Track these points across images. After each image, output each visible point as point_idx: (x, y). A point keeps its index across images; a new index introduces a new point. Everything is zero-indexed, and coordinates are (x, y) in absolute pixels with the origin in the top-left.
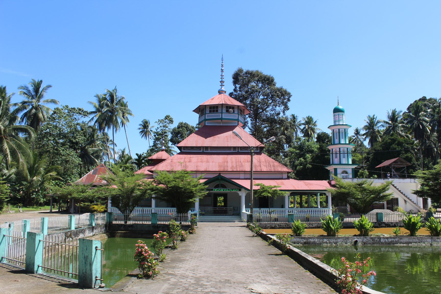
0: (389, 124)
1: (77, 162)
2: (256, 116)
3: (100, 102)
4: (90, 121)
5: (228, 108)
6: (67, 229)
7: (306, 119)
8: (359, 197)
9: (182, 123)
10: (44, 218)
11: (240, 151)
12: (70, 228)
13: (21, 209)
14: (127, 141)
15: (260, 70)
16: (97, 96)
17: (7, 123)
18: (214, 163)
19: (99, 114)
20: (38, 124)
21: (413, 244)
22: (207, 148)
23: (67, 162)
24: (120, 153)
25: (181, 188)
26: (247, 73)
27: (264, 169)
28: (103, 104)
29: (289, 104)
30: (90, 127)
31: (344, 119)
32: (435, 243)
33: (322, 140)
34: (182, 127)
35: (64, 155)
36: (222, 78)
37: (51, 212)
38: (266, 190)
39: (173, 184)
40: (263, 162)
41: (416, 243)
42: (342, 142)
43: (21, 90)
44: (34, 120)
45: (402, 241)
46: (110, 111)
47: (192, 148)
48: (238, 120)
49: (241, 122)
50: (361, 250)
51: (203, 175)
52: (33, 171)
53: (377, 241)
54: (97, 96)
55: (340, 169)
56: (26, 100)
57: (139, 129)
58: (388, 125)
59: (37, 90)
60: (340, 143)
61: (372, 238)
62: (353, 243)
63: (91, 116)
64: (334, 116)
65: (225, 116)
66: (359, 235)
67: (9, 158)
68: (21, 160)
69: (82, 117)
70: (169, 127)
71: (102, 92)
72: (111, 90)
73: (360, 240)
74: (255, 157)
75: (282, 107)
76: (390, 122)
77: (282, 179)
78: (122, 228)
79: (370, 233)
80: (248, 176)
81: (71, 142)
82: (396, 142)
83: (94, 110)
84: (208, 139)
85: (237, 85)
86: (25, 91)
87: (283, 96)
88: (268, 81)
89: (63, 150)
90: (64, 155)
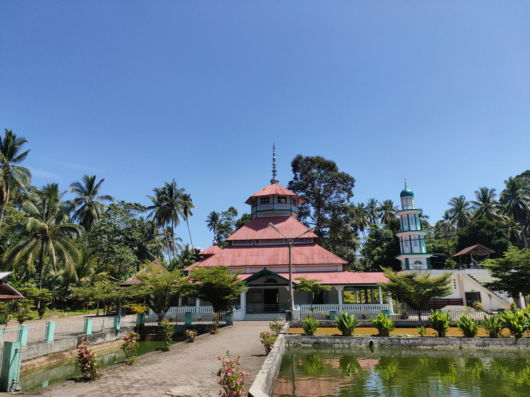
0: (480, 205)
1: (132, 259)
2: (319, 205)
3: (159, 195)
4: (147, 216)
5: (280, 198)
6: (81, 333)
7: (383, 205)
8: (412, 291)
9: (246, 215)
10: (49, 323)
11: (233, 245)
12: (85, 333)
13: (66, 314)
14: (193, 233)
15: (321, 156)
16: (156, 190)
17: (54, 222)
18: (264, 257)
19: (157, 208)
20: (91, 221)
21: (438, 346)
22: (257, 241)
23: (121, 260)
24: (184, 248)
25: (215, 284)
26: (307, 159)
27: (317, 261)
28: (162, 198)
29: (353, 190)
30: (149, 222)
31: (413, 203)
32: (466, 345)
33: (396, 226)
34: (246, 218)
35: (118, 253)
36: (274, 168)
37: (98, 316)
38: (306, 285)
39: (206, 280)
40: (318, 254)
41: (442, 345)
42: (413, 228)
43: (73, 187)
44: (87, 218)
45: (425, 342)
46: (170, 204)
47: (243, 241)
48: (291, 210)
49: (295, 212)
50: (378, 352)
51: (248, 270)
52: (82, 271)
53: (397, 344)
54: (156, 190)
55: (412, 259)
56: (79, 197)
57: (208, 221)
58: (479, 207)
59: (90, 186)
60: (410, 230)
61: (390, 339)
62: (368, 345)
63: (149, 212)
64: (402, 200)
65: (277, 206)
66: (378, 336)
67: (55, 258)
68: (67, 260)
69: (139, 212)
70: (233, 220)
71: (161, 186)
72: (170, 184)
73: (376, 341)
74: (294, 249)
75: (346, 194)
76: (481, 203)
77: (337, 271)
78: (154, 330)
79: (391, 333)
80: (287, 270)
81: (127, 238)
82: (486, 226)
83: (153, 205)
84: (259, 231)
85: (297, 173)
86: (77, 188)
87: (347, 182)
88: (330, 167)
89: (118, 248)
90: (118, 253)
